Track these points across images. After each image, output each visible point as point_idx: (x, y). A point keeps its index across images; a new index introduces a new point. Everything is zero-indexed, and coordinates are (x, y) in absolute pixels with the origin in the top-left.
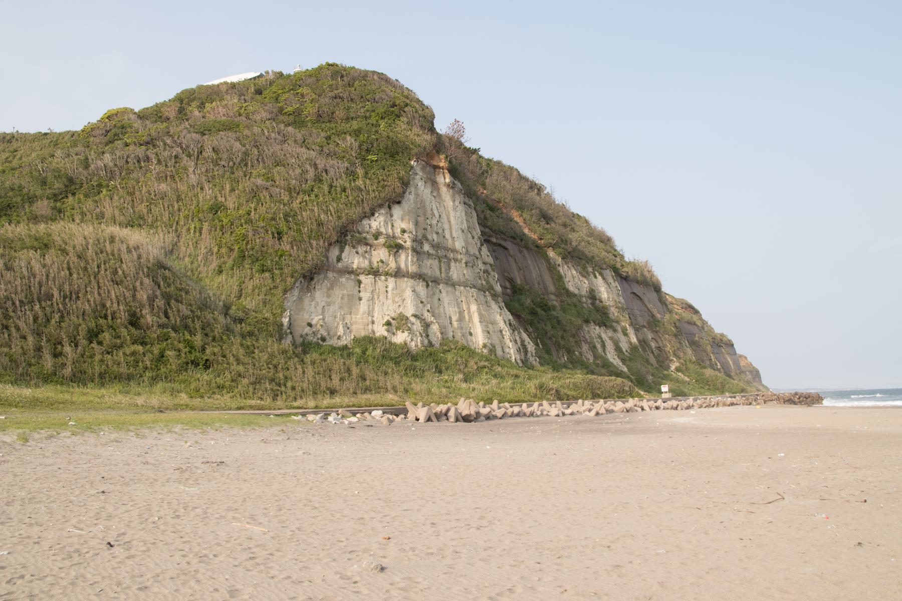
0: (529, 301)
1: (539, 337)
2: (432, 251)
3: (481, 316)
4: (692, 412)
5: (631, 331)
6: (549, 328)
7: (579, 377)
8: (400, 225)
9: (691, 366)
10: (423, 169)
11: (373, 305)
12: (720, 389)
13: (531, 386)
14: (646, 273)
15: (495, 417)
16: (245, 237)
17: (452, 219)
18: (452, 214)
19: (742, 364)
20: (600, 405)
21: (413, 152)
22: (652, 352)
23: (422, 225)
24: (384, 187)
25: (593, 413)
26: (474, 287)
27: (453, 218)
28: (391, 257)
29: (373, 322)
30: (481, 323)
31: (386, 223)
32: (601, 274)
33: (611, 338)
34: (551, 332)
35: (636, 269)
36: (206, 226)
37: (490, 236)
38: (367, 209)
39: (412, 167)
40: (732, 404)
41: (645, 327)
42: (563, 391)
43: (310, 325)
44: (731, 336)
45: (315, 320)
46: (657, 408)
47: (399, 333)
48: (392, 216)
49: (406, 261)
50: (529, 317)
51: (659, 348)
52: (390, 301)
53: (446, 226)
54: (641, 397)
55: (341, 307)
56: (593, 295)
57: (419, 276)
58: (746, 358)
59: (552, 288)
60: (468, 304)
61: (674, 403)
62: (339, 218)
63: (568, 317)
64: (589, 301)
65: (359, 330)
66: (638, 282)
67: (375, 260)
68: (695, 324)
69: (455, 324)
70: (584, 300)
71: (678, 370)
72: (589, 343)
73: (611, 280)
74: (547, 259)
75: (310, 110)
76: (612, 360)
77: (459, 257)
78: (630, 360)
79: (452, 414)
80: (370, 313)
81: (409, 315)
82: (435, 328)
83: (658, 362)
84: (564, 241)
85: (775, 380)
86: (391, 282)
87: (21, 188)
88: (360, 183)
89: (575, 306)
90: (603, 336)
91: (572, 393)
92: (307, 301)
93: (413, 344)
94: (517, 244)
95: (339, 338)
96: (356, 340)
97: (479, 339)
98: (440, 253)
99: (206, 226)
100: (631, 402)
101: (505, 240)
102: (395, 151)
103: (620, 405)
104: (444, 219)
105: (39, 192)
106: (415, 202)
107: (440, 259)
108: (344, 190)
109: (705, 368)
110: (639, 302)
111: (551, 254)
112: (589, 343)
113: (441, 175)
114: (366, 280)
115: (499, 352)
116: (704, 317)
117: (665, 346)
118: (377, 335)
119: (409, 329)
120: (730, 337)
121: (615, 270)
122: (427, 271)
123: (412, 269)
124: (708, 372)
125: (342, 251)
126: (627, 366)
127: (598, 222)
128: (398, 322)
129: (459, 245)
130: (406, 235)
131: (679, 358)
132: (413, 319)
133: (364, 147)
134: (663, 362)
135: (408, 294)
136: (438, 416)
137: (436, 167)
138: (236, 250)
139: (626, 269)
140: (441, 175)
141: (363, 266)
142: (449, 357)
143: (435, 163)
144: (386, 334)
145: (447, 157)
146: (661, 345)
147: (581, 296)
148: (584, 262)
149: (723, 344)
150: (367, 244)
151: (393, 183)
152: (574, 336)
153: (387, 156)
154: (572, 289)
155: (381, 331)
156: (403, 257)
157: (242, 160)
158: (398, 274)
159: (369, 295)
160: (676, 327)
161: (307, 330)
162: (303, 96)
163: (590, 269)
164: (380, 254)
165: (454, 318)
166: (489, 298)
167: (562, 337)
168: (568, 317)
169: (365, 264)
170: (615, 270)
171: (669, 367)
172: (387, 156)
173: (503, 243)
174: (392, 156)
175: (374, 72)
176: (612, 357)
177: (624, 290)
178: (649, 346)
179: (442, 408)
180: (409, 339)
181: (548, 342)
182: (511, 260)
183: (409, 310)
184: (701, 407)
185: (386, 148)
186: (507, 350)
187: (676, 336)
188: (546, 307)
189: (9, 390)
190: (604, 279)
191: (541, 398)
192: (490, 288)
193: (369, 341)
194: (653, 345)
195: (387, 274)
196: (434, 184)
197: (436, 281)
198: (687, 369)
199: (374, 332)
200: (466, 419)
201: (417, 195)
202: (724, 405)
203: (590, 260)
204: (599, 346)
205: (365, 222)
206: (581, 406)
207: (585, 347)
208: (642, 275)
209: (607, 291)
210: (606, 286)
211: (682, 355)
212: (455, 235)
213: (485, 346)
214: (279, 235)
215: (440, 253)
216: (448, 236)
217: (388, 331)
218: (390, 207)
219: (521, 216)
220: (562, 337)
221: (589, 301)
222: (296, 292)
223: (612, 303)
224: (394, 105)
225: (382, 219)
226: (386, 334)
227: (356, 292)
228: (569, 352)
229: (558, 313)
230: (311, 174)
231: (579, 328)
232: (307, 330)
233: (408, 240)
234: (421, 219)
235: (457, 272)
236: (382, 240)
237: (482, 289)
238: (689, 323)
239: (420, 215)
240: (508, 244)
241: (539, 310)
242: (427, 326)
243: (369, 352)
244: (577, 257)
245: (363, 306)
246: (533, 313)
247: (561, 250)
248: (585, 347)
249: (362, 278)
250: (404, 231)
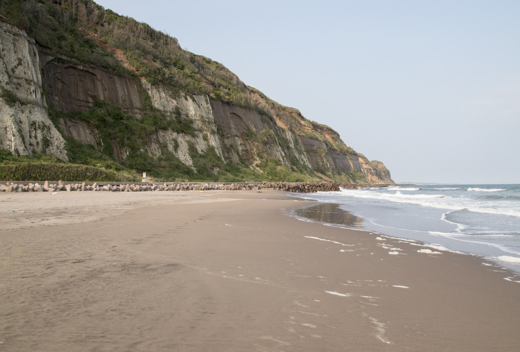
19: (380, 166)
22: (238, 153)
37: (77, 64)
41: (237, 136)
56: (177, 112)
58: (382, 163)
59: (137, 104)
64: (174, 115)
68: (317, 139)
74: (140, 85)
111: (144, 80)
117: (252, 149)
131: (261, 157)
146: (248, 148)
154: (156, 105)
189: (3, 187)
210: (195, 106)
221: (174, 115)
223: (198, 118)
238: (311, 138)
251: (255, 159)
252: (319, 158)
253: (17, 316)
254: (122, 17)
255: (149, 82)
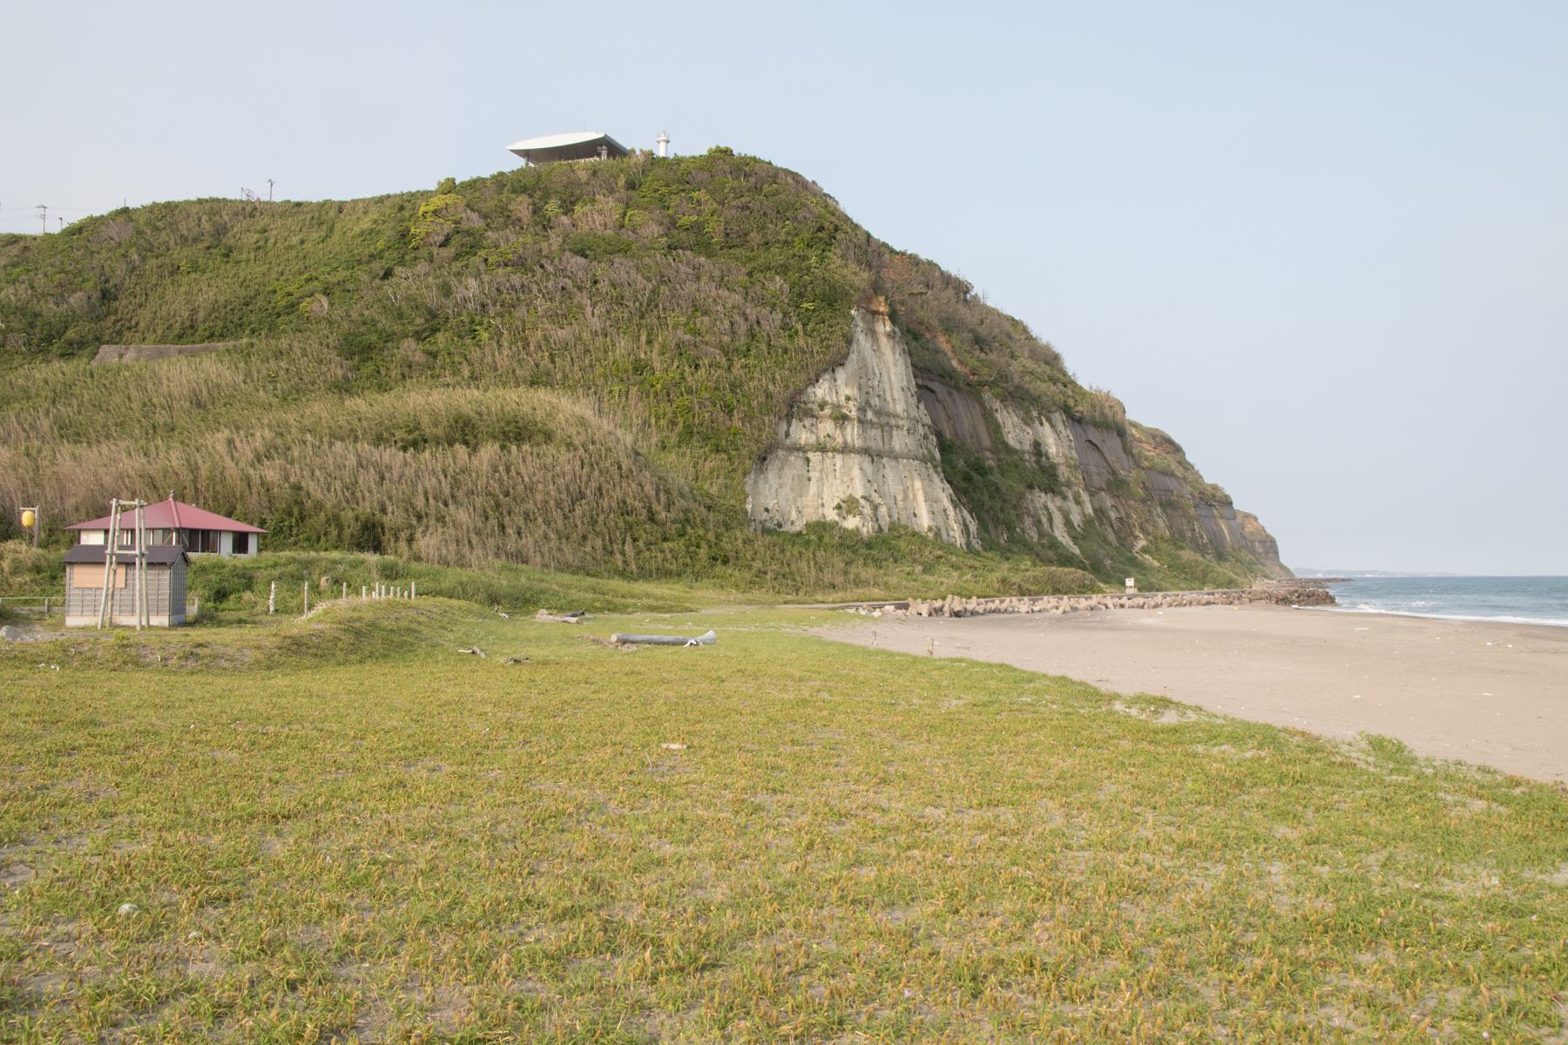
0: (961, 463)
1: (976, 509)
3: (926, 494)
4: (1160, 612)
5: (1085, 497)
6: (986, 498)
8: (846, 391)
9: (1163, 546)
11: (820, 486)
13: (994, 578)
14: (1107, 410)
16: (689, 409)
19: (1249, 528)
20: (1066, 602)
23: (865, 389)
24: (828, 347)
27: (891, 369)
30: (926, 503)
32: (1049, 420)
33: (1060, 509)
34: (988, 504)
35: (1093, 406)
36: (634, 390)
38: (812, 375)
40: (1208, 603)
41: (1101, 489)
43: (767, 510)
45: (771, 504)
46: (1122, 606)
47: (850, 517)
49: (852, 434)
50: (963, 484)
51: (1120, 519)
53: (887, 386)
54: (1100, 591)
57: (865, 451)
58: (1255, 519)
59: (987, 442)
61: (1140, 601)
62: (787, 387)
63: (1010, 482)
65: (811, 515)
66: (1096, 425)
67: (822, 434)
68: (1172, 475)
69: (900, 504)
70: (1027, 457)
71: (1145, 550)
73: (1061, 427)
75: (714, 228)
78: (1084, 538)
79: (946, 609)
80: (820, 495)
82: (883, 510)
83: (1119, 539)
84: (1004, 377)
86: (839, 458)
87: (374, 322)
88: (801, 341)
90: (1050, 505)
91: (1033, 588)
92: (761, 482)
94: (946, 384)
96: (808, 525)
97: (924, 521)
98: (884, 420)
99: (634, 390)
100: (1095, 599)
102: (833, 299)
103: (1083, 603)
104: (885, 378)
105: (397, 328)
107: (882, 426)
108: (786, 351)
109: (1182, 548)
110: (1096, 454)
114: (815, 457)
115: (944, 536)
116: (1189, 458)
117: (1128, 516)
120: (1227, 491)
121: (1067, 410)
122: (872, 444)
123: (858, 443)
125: (789, 425)
128: (848, 506)
129: (900, 408)
132: (862, 502)
133: (796, 290)
134: (1124, 535)
135: (856, 472)
136: (939, 611)
137: (875, 313)
138: (681, 425)
139: (1080, 408)
142: (902, 544)
147: (1023, 452)
148: (1027, 404)
149: (1215, 501)
151: (837, 341)
152: (1015, 507)
154: (1012, 442)
155: (832, 515)
156: (849, 429)
157: (650, 300)
158: (845, 450)
160: (1145, 488)
161: (765, 516)
162: (699, 203)
163: (1035, 414)
164: (827, 427)
165: (900, 498)
167: (1002, 509)
169: (812, 439)
170: (1067, 410)
171: (1133, 546)
173: (930, 384)
175: (787, 172)
177: (1076, 438)
178: (1108, 518)
179: (938, 604)
181: (985, 516)
182: (939, 406)
183: (858, 493)
184: (1170, 605)
187: (1144, 501)
188: (981, 469)
190: (1052, 426)
191: (1005, 594)
192: (933, 459)
194: (1113, 515)
195: (834, 450)
197: (880, 455)
198: (1158, 550)
200: (957, 614)
202: (1199, 603)
203: (1035, 400)
204: (1044, 520)
205: (810, 390)
206: (1048, 602)
207: (1028, 521)
208: (1102, 413)
209: (1056, 442)
211: (1150, 528)
213: (930, 529)
214: (729, 410)
215: (884, 420)
219: (948, 341)
220: (1002, 509)
222: (753, 476)
223: (1061, 460)
224: (821, 229)
225: (826, 385)
228: (1010, 528)
229: (995, 477)
230: (742, 328)
231: (1021, 496)
232: (765, 516)
236: (827, 411)
237: (924, 460)
239: (864, 378)
241: (973, 473)
242: (875, 508)
243: (826, 539)
245: (813, 488)
246: (967, 478)
248: (1028, 521)
249: (810, 455)
250: (848, 399)
251: (1136, 537)
252: (1184, 521)
253: (471, 547)
254: (903, 254)
255: (996, 397)
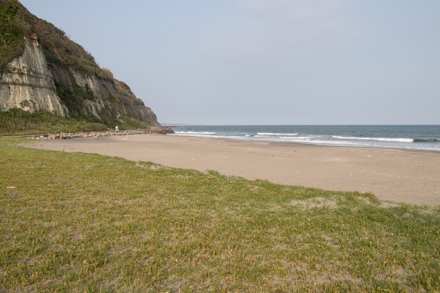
2: (33, 75)
3: (51, 99)
5: (102, 102)
6: (71, 101)
7: (89, 124)
9: (125, 117)
10: (28, 41)
12: (135, 126)
14: (108, 75)
15: (71, 138)
17: (39, 61)
18: (39, 59)
20: (98, 134)
21: (25, 33)
24: (16, 49)
25: (97, 136)
26: (48, 88)
27: (39, 59)
28: (20, 78)
29: (15, 103)
30: (51, 103)
31: (17, 64)
32: (90, 78)
33: (94, 105)
38: (10, 58)
39: (25, 40)
40: (140, 134)
41: (107, 99)
42: (85, 129)
44: (144, 100)
46: (115, 135)
47: (26, 107)
48: (19, 61)
49: (25, 79)
52: (21, 95)
53: (37, 64)
54: (108, 130)
55: (4, 97)
56: (87, 86)
57: (30, 85)
58: (150, 109)
59: (71, 84)
60: (47, 95)
61: (120, 133)
63: (78, 97)
65: (11, 106)
66: (105, 80)
67: (14, 79)
68: (127, 95)
70: (84, 89)
71: (120, 118)
72: (86, 107)
73: (94, 80)
76: (94, 114)
77: (42, 76)
78: (102, 114)
79: (61, 136)
80: (14, 99)
81: (28, 100)
82: (37, 105)
83: (112, 114)
84: (76, 63)
85: (163, 120)
89: (80, 92)
90: (91, 104)
93: (31, 111)
94: (57, 64)
95: (4, 109)
96: (10, 109)
98: (36, 75)
100: (107, 133)
101: (52, 63)
103: (103, 134)
106: (27, 55)
107: (36, 77)
109: (131, 117)
110: (105, 89)
112: (86, 107)
113: (35, 42)
114: (12, 87)
116: (132, 91)
117: (115, 108)
118: (18, 107)
119: (29, 106)
121: (96, 75)
122: (33, 83)
123: (27, 82)
124: (132, 119)
126: (101, 117)
127: (88, 49)
128: (25, 103)
129: (42, 71)
130: (25, 69)
131: (120, 113)
132: (30, 102)
135: (27, 92)
137: (33, 39)
140: (35, 42)
141: (10, 81)
142: (44, 116)
143: (32, 37)
144: (21, 107)
145: (36, 35)
147: (82, 87)
149: (139, 103)
150: (11, 73)
151: (19, 48)
152: (80, 105)
153: (14, 34)
154: (79, 84)
155: (19, 106)
158: (23, 84)
159: (13, 92)
163: (86, 75)
164: (16, 77)
165: (43, 101)
166: (53, 92)
167: (76, 105)
168: (78, 97)
169: (11, 80)
170: (96, 75)
171: (116, 117)
172: (14, 34)
174: (16, 35)
176: (95, 113)
178: (109, 108)
179: (58, 135)
180: (29, 109)
181: (71, 107)
182: (55, 71)
183: (28, 99)
184: (129, 134)
185: (13, 31)
186: (60, 112)
187: (119, 103)
190: (92, 79)
191: (79, 131)
192: (53, 89)
193: (15, 111)
194: (110, 107)
195: (19, 84)
196: (32, 46)
198: (124, 118)
199: (16, 106)
200: (64, 138)
201: (27, 52)
202: (137, 134)
203: (86, 71)
204: (89, 109)
205: (9, 63)
206: (93, 134)
207: (84, 109)
208: (107, 76)
209: (92, 85)
211: (121, 111)
212: (41, 67)
213: (53, 111)
215: (36, 75)
216: (38, 68)
217: (21, 106)
218: (18, 58)
220: (76, 105)
223: (94, 90)
224: (11, 7)
225: (15, 62)
226: (21, 107)
227: (8, 92)
228: (79, 111)
229: (74, 95)
231: (82, 101)
233: (26, 71)
234: (29, 62)
235: (42, 82)
236: (16, 71)
237: (50, 89)
239: (29, 60)
240: (53, 65)
241: (66, 93)
242: (34, 104)
244: (82, 71)
245: (12, 97)
247: (75, 67)
249: (10, 86)
